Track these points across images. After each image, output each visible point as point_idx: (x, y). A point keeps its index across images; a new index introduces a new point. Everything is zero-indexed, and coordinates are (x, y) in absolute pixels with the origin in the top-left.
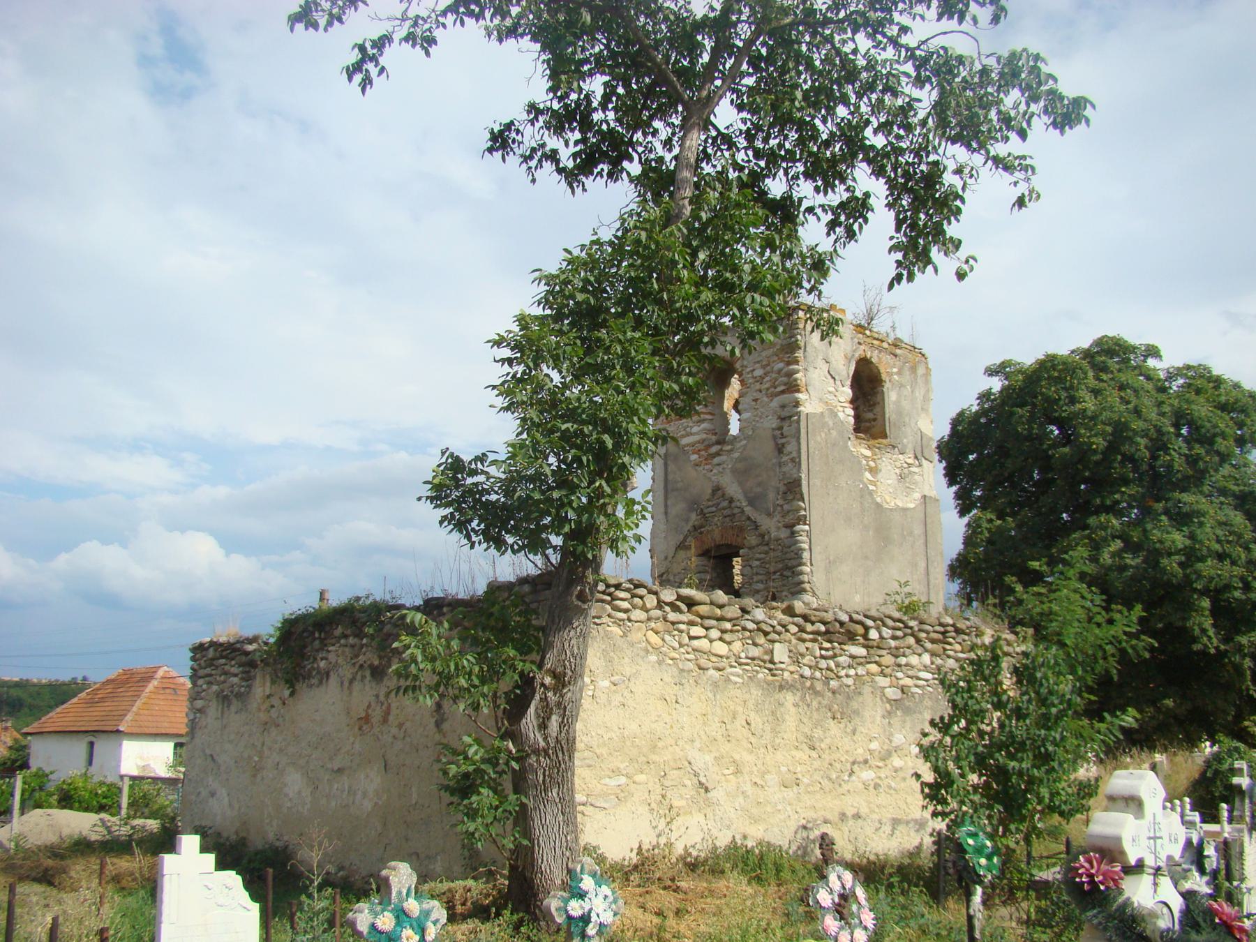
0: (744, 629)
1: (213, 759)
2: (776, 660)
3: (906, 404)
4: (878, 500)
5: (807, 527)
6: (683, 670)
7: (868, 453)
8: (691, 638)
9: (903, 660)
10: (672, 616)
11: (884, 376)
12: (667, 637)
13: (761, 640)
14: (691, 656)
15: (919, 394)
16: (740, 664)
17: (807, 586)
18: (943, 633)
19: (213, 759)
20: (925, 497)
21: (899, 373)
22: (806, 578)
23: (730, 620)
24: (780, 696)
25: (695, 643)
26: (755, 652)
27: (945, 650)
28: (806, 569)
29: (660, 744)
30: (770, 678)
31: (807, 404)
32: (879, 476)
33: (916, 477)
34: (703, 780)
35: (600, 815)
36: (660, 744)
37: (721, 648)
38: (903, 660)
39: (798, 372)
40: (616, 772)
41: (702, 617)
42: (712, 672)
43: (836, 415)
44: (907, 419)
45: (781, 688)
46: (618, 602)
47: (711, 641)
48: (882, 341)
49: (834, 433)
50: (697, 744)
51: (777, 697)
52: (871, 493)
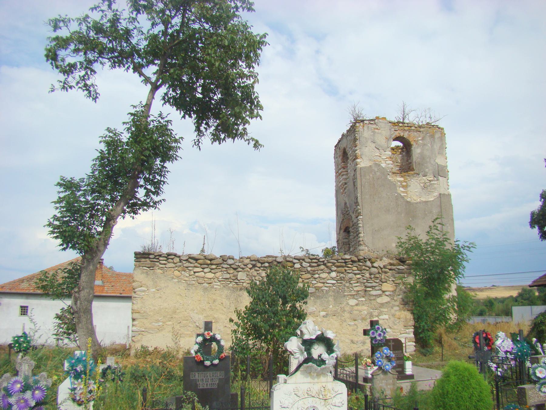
0: (223, 267)
1: (522, 317)
2: (239, 279)
3: (427, 153)
4: (409, 200)
5: (361, 217)
6: (189, 284)
7: (402, 179)
8: (195, 272)
9: (316, 276)
10: (187, 264)
11: (412, 143)
12: (183, 272)
13: (232, 271)
14: (195, 279)
15: (436, 146)
16: (220, 281)
17: (362, 243)
18: (345, 262)
19: (522, 317)
20: (440, 194)
21: (422, 140)
22: (361, 239)
23: (215, 265)
24: (241, 293)
25: (197, 274)
26: (228, 276)
27: (345, 270)
28: (361, 235)
29: (178, 311)
30: (236, 286)
31: (361, 164)
32: (409, 189)
33: (435, 186)
34: (198, 324)
35: (150, 335)
36: (178, 311)
37: (211, 275)
38: (316, 276)
39: (357, 150)
40: (158, 321)
41: (201, 264)
42: (205, 284)
43: (379, 165)
44: (428, 160)
45: (241, 289)
46: (161, 262)
47: (205, 273)
48: (411, 127)
49: (378, 174)
50: (195, 311)
51: (238, 293)
52: (403, 197)
